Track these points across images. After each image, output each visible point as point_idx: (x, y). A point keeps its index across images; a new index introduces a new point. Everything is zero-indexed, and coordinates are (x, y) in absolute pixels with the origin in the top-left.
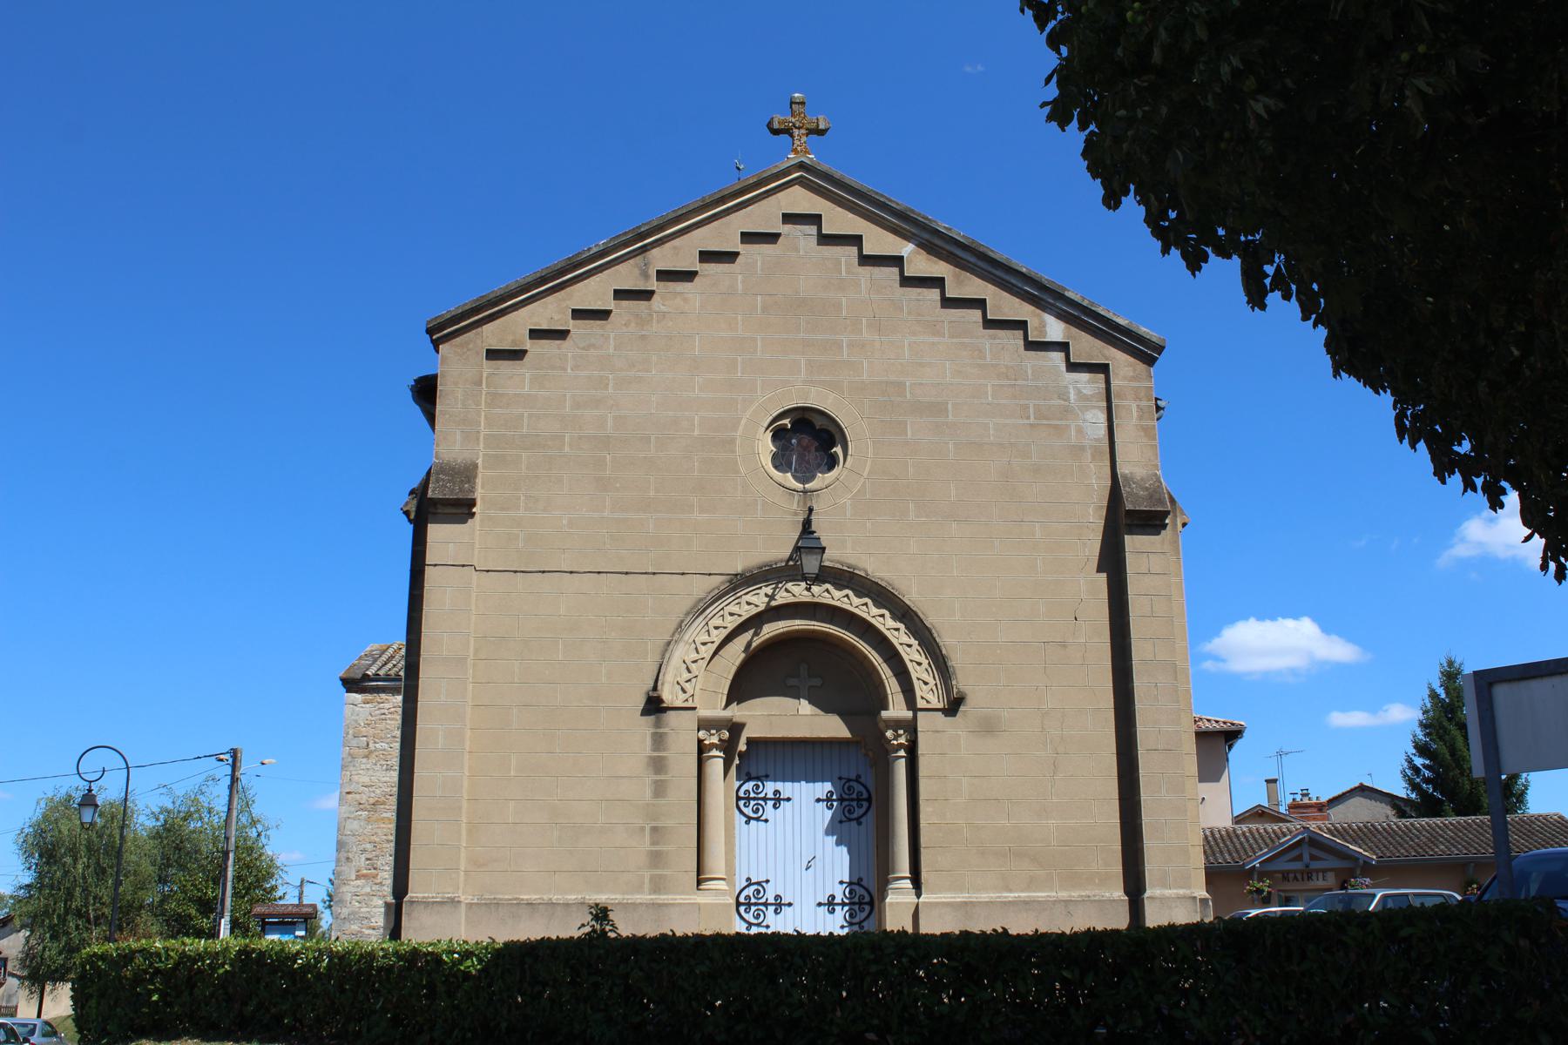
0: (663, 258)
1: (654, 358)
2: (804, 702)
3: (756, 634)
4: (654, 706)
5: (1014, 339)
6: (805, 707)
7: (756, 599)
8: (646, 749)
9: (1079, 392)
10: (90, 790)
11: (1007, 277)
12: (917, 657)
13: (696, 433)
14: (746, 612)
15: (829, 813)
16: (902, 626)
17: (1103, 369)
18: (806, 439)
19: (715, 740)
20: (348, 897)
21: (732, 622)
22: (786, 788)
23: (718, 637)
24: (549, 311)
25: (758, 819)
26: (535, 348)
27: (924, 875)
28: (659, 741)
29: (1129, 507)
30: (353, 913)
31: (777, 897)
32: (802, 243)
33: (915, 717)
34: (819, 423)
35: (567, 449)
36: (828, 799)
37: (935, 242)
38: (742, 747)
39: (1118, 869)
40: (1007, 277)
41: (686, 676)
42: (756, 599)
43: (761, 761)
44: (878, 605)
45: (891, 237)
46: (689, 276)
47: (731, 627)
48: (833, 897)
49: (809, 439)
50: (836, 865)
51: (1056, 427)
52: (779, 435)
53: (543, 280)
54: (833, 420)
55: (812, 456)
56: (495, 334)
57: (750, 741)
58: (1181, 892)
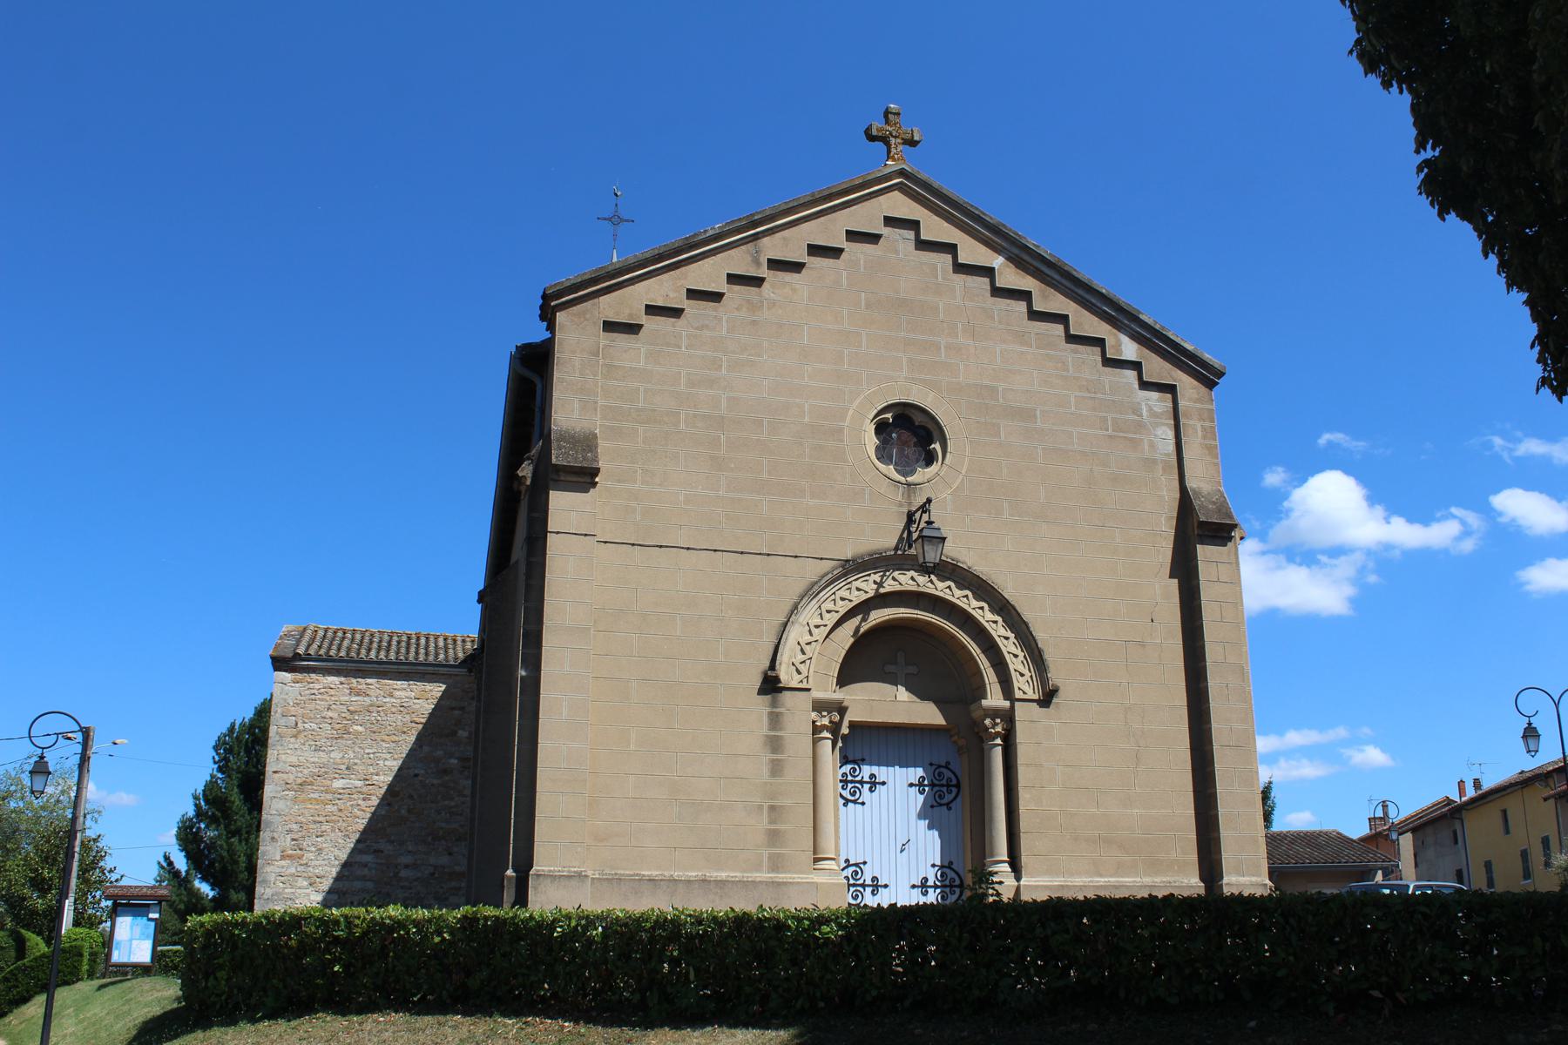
0: (774, 247)
1: (765, 344)
3: (864, 620)
4: (771, 685)
5: (1093, 354)
6: (902, 694)
7: (866, 586)
8: (763, 728)
9: (1150, 409)
10: (42, 757)
11: (1088, 297)
12: (1013, 649)
13: (806, 420)
14: (858, 597)
15: (921, 798)
17: (1171, 389)
18: (906, 435)
19: (826, 721)
20: (272, 878)
21: (844, 607)
22: (882, 772)
23: (830, 620)
24: (665, 289)
25: (855, 802)
26: (652, 324)
27: (1025, 859)
28: (775, 720)
29: (1202, 519)
30: (277, 894)
31: (874, 879)
32: (901, 246)
33: (1012, 707)
34: (918, 419)
35: (682, 426)
36: (921, 784)
37: (1023, 256)
38: (845, 730)
39: (1194, 857)
40: (1088, 297)
41: (801, 657)
42: (866, 586)
43: (865, 744)
44: (978, 598)
45: (982, 249)
46: (797, 267)
47: (842, 611)
48: (926, 879)
49: (910, 433)
50: (927, 850)
51: (1131, 440)
52: (881, 428)
54: (933, 418)
55: (910, 451)
56: (613, 306)
57: (852, 725)
58: (1254, 879)
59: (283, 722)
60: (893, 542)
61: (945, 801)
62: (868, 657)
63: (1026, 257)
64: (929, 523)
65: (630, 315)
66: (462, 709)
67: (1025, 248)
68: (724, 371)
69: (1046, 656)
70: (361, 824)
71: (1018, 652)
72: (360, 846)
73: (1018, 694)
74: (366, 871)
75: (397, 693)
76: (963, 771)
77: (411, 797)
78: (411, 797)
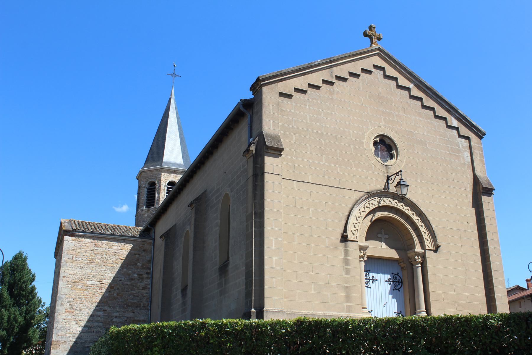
2: (384, 244)
3: (374, 216)
4: (344, 239)
6: (384, 245)
9: (462, 145)
14: (373, 207)
15: (390, 286)
16: (419, 219)
17: (468, 138)
18: (383, 147)
20: (61, 320)
22: (376, 276)
24: (301, 82)
26: (296, 95)
28: (346, 253)
30: (63, 327)
33: (425, 252)
34: (388, 141)
36: (389, 281)
41: (354, 229)
42: (374, 203)
43: (373, 264)
44: (412, 210)
49: (385, 146)
51: (457, 156)
52: (375, 143)
53: (299, 70)
55: (385, 153)
59: (67, 256)
60: (382, 187)
61: (398, 288)
62: (378, 229)
63: (421, 85)
64: (401, 179)
65: (289, 91)
66: (139, 254)
67: (421, 82)
68: (322, 116)
69: (436, 234)
70: (98, 299)
71: (426, 231)
72: (97, 308)
73: (427, 248)
74: (99, 318)
75: (114, 247)
76: (406, 275)
77: (118, 289)
78: (118, 289)
